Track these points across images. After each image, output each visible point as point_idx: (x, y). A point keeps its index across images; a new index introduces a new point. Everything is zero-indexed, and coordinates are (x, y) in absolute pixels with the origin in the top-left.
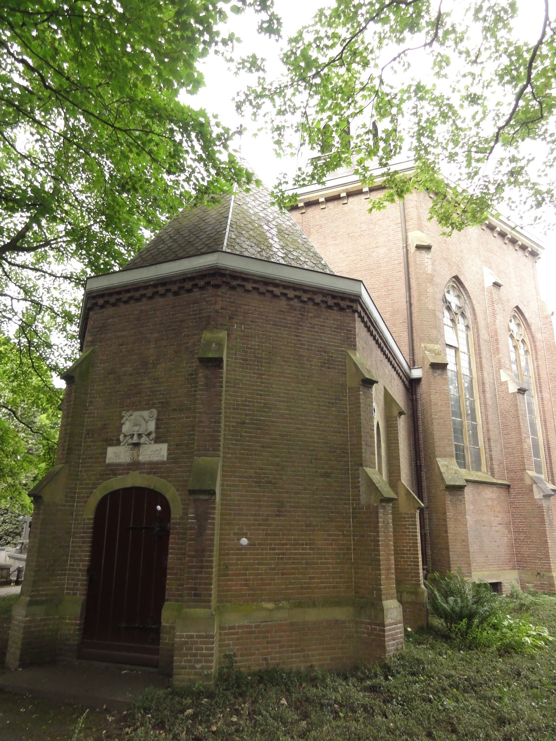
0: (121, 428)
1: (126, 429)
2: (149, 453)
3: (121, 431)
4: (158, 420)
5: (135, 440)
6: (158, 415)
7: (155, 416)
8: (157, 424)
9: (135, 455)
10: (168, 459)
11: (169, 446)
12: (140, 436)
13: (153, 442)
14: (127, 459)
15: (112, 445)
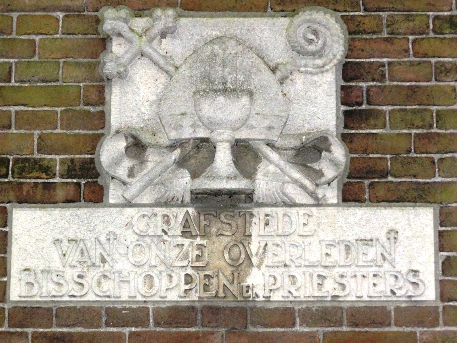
0: (101, 100)
1: (133, 101)
2: (315, 254)
3: (102, 119)
4: (350, 71)
5: (223, 172)
6: (351, 50)
7: (337, 49)
8: (346, 95)
9: (219, 261)
10: (443, 295)
11: (443, 218)
12: (245, 154)
13: (332, 195)
14: (161, 283)
15: (43, 197)
